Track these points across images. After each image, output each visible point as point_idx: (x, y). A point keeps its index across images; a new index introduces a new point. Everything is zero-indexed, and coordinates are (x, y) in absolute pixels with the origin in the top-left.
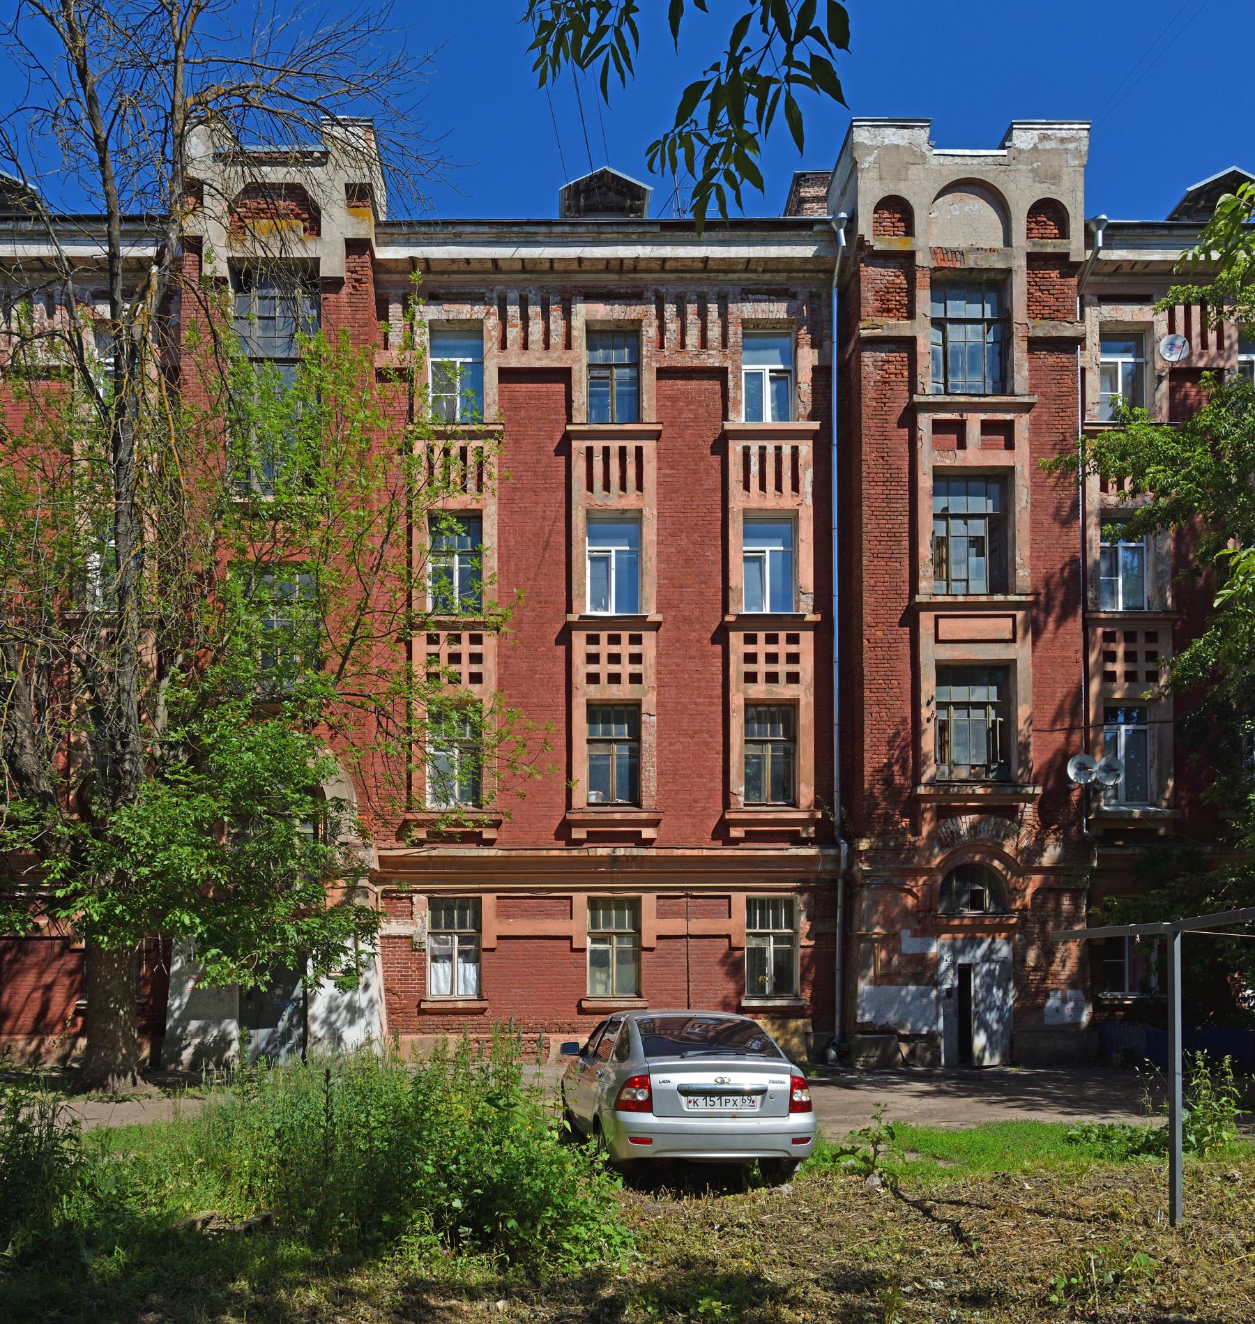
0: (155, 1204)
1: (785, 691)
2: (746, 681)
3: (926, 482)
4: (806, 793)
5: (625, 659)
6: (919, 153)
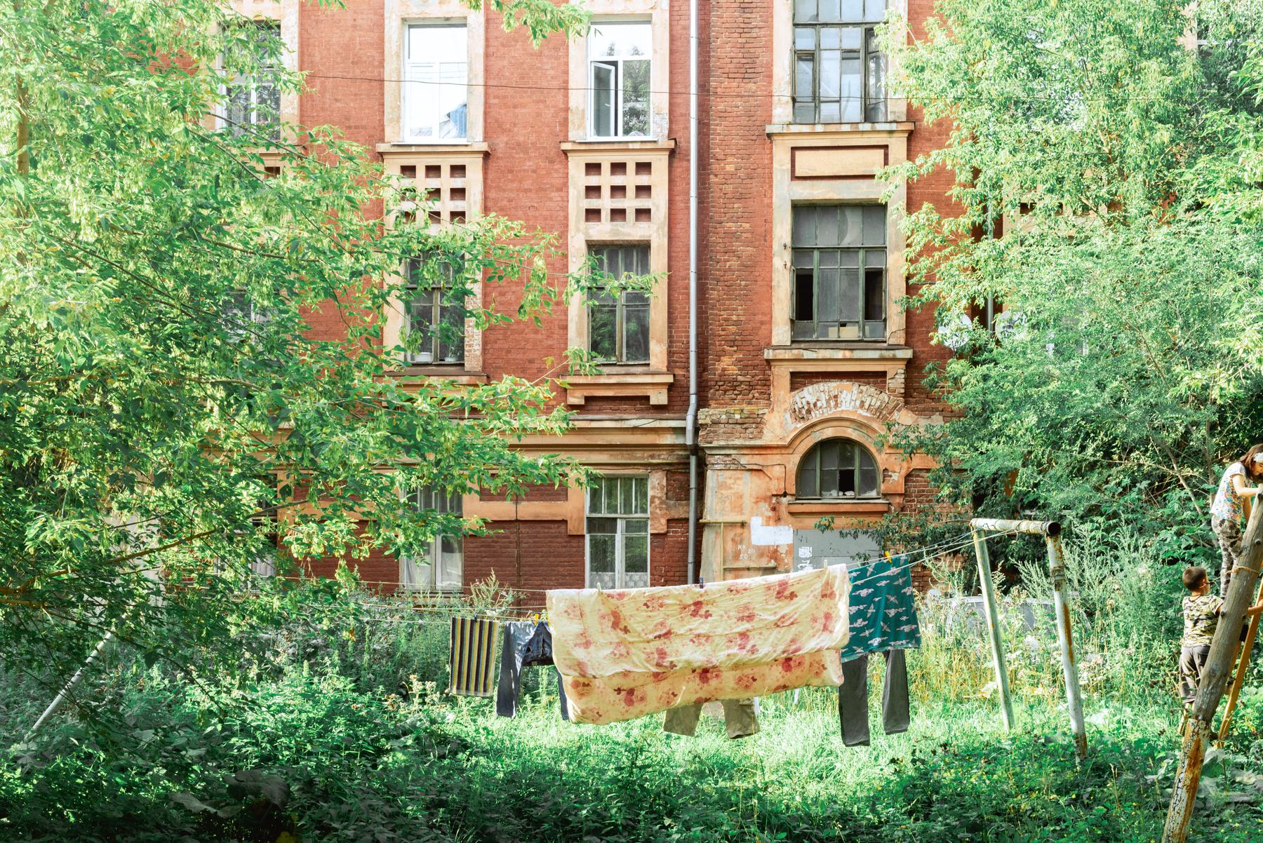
1: (631, 231)
2: (587, 220)
3: (658, 259)
4: (658, 352)
5: (446, 194)
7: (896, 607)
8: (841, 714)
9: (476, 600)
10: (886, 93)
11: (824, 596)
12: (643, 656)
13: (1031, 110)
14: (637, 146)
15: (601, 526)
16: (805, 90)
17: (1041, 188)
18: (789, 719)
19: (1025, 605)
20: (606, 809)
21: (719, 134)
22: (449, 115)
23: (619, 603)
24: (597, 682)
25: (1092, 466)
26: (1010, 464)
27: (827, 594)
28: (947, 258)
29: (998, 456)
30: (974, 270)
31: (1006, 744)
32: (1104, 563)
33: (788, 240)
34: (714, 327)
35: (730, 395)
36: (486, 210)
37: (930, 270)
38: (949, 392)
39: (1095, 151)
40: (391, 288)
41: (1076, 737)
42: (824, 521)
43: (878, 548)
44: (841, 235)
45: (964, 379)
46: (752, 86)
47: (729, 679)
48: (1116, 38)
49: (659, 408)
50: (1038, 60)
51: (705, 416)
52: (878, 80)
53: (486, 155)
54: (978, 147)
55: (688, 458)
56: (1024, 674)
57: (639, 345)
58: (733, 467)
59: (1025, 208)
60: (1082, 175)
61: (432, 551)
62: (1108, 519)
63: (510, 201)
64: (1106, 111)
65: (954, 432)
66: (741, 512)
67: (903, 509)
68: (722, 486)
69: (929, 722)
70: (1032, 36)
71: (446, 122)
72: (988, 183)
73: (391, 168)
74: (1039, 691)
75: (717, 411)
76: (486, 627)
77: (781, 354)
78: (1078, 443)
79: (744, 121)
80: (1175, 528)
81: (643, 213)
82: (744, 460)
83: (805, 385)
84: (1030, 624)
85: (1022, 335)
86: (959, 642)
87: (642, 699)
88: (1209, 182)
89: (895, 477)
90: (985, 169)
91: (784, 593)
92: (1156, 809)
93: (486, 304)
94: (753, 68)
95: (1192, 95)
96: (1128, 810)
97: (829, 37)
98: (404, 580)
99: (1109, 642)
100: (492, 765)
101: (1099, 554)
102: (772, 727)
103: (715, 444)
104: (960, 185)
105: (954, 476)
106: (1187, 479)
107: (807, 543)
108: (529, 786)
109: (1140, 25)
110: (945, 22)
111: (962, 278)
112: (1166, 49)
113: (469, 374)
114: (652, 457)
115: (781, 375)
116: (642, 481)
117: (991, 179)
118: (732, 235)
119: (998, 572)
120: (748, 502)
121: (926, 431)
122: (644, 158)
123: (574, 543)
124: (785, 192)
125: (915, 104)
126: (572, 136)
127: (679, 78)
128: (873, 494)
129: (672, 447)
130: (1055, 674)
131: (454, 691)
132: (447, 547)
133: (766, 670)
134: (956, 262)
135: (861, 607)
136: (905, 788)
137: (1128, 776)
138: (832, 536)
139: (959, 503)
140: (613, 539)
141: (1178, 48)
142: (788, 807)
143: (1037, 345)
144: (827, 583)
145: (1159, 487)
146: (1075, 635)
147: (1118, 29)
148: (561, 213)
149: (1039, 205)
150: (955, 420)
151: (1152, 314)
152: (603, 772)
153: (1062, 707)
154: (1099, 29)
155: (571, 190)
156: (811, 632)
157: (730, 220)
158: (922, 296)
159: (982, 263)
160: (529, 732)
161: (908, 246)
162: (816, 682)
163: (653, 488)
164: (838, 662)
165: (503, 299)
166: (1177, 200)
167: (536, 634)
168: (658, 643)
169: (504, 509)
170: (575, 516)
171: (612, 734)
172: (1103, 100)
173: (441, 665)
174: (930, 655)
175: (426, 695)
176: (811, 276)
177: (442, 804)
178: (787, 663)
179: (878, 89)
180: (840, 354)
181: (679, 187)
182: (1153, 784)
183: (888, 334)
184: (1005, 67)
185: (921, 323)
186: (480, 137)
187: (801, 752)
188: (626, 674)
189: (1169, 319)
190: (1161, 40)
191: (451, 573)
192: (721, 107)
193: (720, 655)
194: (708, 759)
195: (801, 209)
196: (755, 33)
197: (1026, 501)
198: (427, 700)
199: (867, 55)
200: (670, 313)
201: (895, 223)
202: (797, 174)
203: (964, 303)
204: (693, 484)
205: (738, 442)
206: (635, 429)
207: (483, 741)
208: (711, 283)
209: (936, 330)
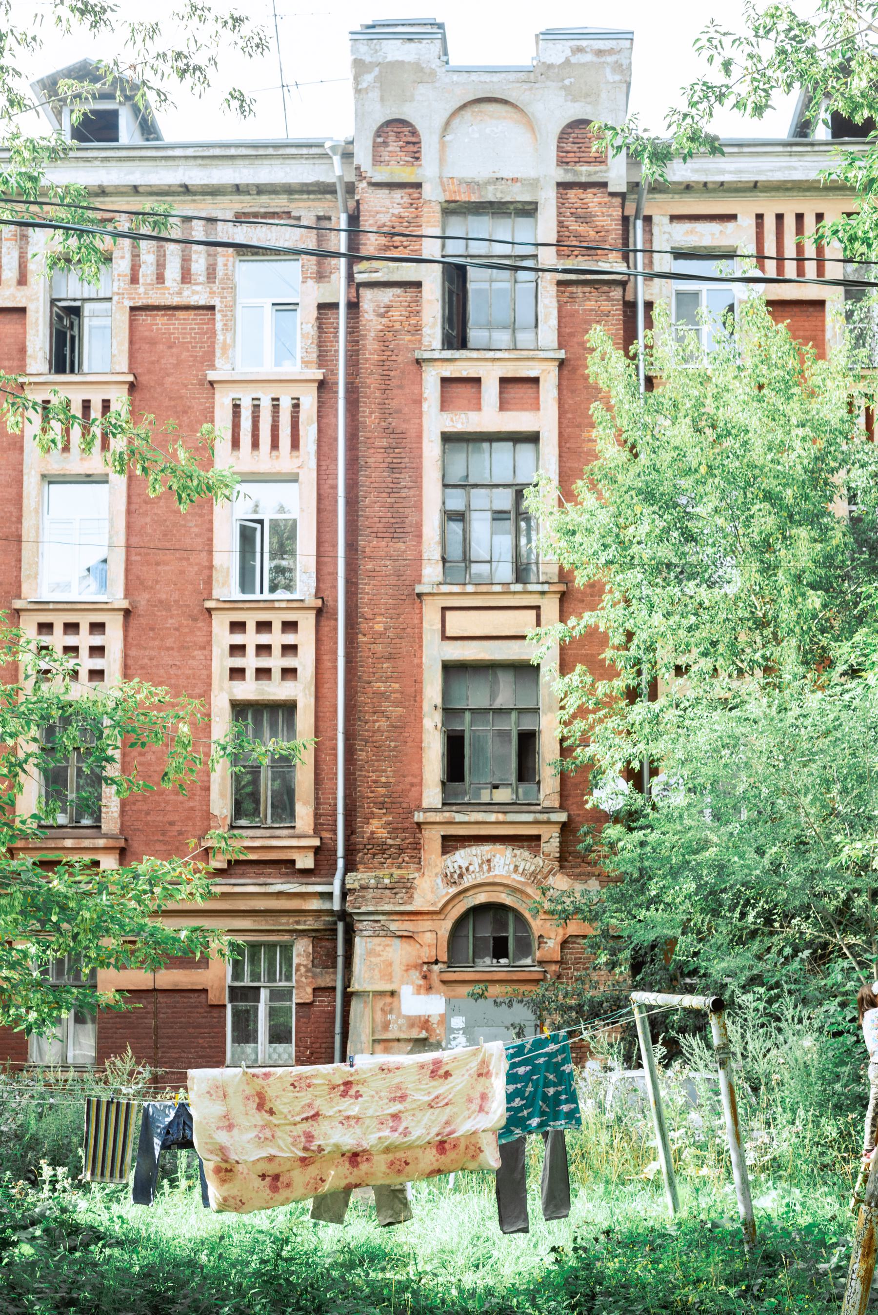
1: (277, 690)
2: (231, 678)
3: (305, 719)
4: (304, 813)
7: (555, 1085)
12: (290, 1140)
14: (283, 605)
15: (244, 995)
16: (455, 552)
17: (695, 651)
18: (444, 1203)
19: (688, 1080)
20: (250, 1306)
23: (264, 1083)
24: (240, 1168)
25: (753, 934)
26: (670, 933)
28: (601, 721)
29: (654, 924)
30: (629, 733)
31: (672, 1230)
32: (768, 1035)
34: (362, 789)
35: (379, 859)
36: (127, 675)
37: (584, 733)
38: (605, 857)
39: (747, 615)
40: (28, 755)
41: (744, 1224)
42: (478, 989)
43: (533, 1017)
44: (493, 696)
45: (620, 844)
46: (401, 546)
47: (380, 1163)
48: (766, 506)
49: (305, 872)
51: (354, 880)
52: (529, 541)
53: (127, 613)
54: (631, 609)
55: (335, 924)
56: (688, 1154)
58: (382, 933)
59: (679, 671)
62: (771, 988)
63: (151, 659)
64: (757, 575)
66: (390, 980)
67: (559, 977)
68: (371, 953)
69: (590, 1205)
70: (683, 500)
71: (84, 577)
73: (28, 629)
74: (705, 1171)
75: (365, 876)
76: (123, 1109)
78: (738, 910)
79: (393, 580)
81: (289, 673)
82: (393, 926)
83: (456, 849)
84: (692, 1102)
85: (679, 799)
86: (620, 1119)
88: (866, 656)
89: (551, 944)
91: (438, 1072)
92: (829, 1301)
93: (124, 770)
94: (403, 527)
95: (843, 561)
96: (801, 1303)
97: (479, 498)
98: (34, 1057)
99: (775, 1119)
101: (762, 1026)
103: (363, 909)
105: (612, 943)
106: (850, 947)
107: (460, 1013)
108: (166, 1280)
109: (789, 492)
110: (595, 486)
111: (617, 741)
113: (106, 836)
114: (298, 923)
115: (432, 839)
116: (287, 949)
117: (645, 642)
118: (382, 695)
119: (658, 1045)
122: (290, 617)
124: (435, 653)
125: (567, 567)
127: (327, 537)
128: (528, 961)
129: (318, 913)
130: (719, 1153)
131: (89, 1177)
132: (79, 1019)
133: (419, 1153)
134: (610, 725)
136: (566, 1280)
137: (800, 1265)
138: (485, 1005)
139: (617, 970)
140: (257, 1008)
141: (829, 514)
142: (443, 1302)
143: (694, 811)
144: (483, 1062)
145: (822, 955)
147: (769, 496)
148: (205, 672)
149: (694, 668)
150: (611, 885)
151: (810, 779)
152: (248, 1263)
153: (729, 1188)
154: (749, 495)
155: (214, 649)
156: (466, 1113)
157: (379, 680)
159: (637, 727)
160: (168, 1220)
161: (562, 708)
162: (472, 1165)
163: (299, 955)
166: (831, 664)
167: (177, 1116)
168: (305, 1126)
173: (73, 1147)
174: (590, 1134)
177: (72, 1302)
178: (441, 1146)
179: (530, 551)
180: (493, 817)
181: (326, 647)
182: (825, 1274)
183: (542, 796)
185: (576, 786)
186: (121, 594)
187: (456, 1240)
188: (271, 1159)
190: (811, 507)
191: (83, 1045)
194: (357, 1247)
195: (450, 669)
196: (404, 493)
197: (686, 971)
198: (58, 1186)
199: (518, 516)
200: (317, 775)
201: (548, 685)
202: (448, 634)
203: (620, 766)
204: (340, 951)
205: (387, 908)
206: (280, 894)
207: (117, 1229)
209: (591, 793)
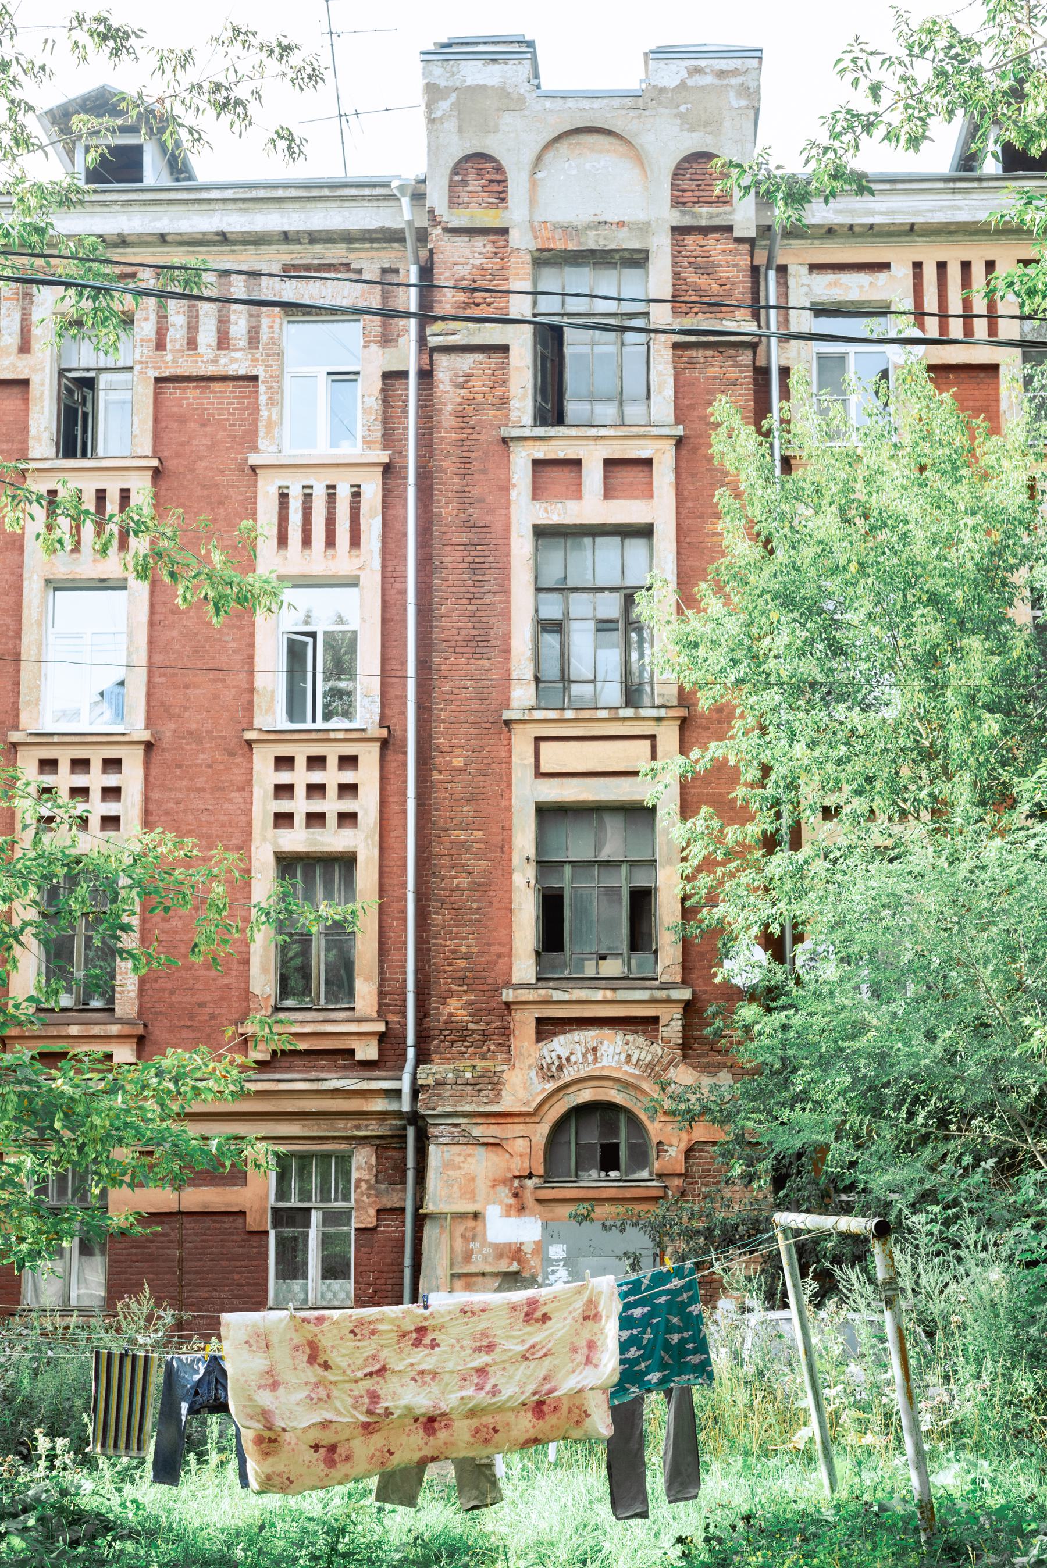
0: (169, 538)
1: (332, 840)
2: (276, 826)
3: (367, 875)
4: (365, 993)
6: (515, 96)
7: (680, 1330)
8: (610, 1475)
9: (124, 1325)
10: (652, 673)
11: (586, 1318)
12: (350, 1401)
13: (834, 693)
14: (341, 735)
15: (289, 1219)
16: (551, 670)
17: (847, 789)
19: (847, 1322)
21: (444, 721)
22: (102, 694)
23: (317, 1329)
24: (287, 1436)
25: (925, 1139)
26: (820, 1138)
27: (590, 1316)
29: (803, 1128)
30: (767, 890)
31: (828, 1514)
33: (531, 851)
34: (438, 961)
35: (459, 1047)
37: (711, 889)
38: (739, 1043)
40: (25, 924)
42: (582, 1209)
43: (651, 1244)
44: (599, 846)
45: (757, 1027)
50: (838, 635)
51: (427, 1074)
52: (642, 656)
53: (149, 746)
54: (768, 738)
55: (404, 1128)
56: (847, 1417)
57: (342, 982)
58: (462, 1140)
59: (827, 813)
60: (897, 773)
61: (67, 1255)
62: (947, 1207)
65: (747, 1095)
66: (473, 1199)
67: (683, 1194)
68: (448, 1165)
69: (725, 1484)
71: (96, 703)
72: (782, 784)
74: (869, 1439)
75: (441, 1068)
76: (141, 1363)
77: (524, 995)
78: (904, 1108)
79: (475, 705)
80: (1033, 1220)
81: (347, 819)
82: (476, 1132)
83: (555, 1034)
85: (830, 971)
86: (761, 1374)
87: (348, 1458)
89: (672, 1152)
90: (777, 765)
91: (534, 1315)
93: (143, 940)
94: (487, 640)
95: (1027, 678)
97: (580, 605)
98: (28, 1298)
99: (955, 1372)
100: (142, 1552)
101: (938, 1254)
102: (517, 1493)
103: (439, 1110)
104: (746, 784)
105: (748, 1151)
107: (560, 1240)
109: (959, 594)
110: (721, 588)
112: (994, 623)
113: (120, 1021)
114: (358, 1128)
115: (524, 1023)
116: (344, 1160)
117: (784, 778)
119: (809, 1280)
120: (482, 1186)
121: (711, 1092)
122: (349, 750)
123: (255, 1241)
124: (527, 793)
125: (688, 687)
126: (258, 723)
127: (393, 652)
128: (645, 1174)
129: (383, 1115)
130: (887, 1416)
132: (85, 1250)
133: (511, 1417)
134: (744, 880)
135: (635, 1332)
139: (755, 1185)
140: (306, 1236)
143: (848, 986)
144: (590, 1301)
146: (912, 1362)
147: (934, 599)
148: (243, 818)
149: (846, 810)
150: (747, 1078)
151: (991, 947)
153: (899, 1461)
154: (910, 598)
155: (256, 790)
158: (701, 921)
159: (776, 882)
160: (194, 1505)
161: (684, 859)
162: (576, 1434)
163: (359, 1168)
164: (605, 1407)
165: (166, 926)
168: (368, 1384)
169: (160, 1197)
170: (256, 1206)
171: (305, 1505)
172: (919, 683)
174: (724, 1393)
175: (55, 1456)
176: (561, 897)
178: (539, 1408)
180: (599, 995)
181: (393, 786)
183: (660, 969)
184: (798, 643)
185: (702, 956)
186: (141, 723)
187: (557, 1528)
188: (325, 1425)
189: (1012, 951)
190: (986, 612)
191: (90, 1282)
192: (446, 688)
193: (451, 1397)
196: (488, 598)
198: (57, 1463)
199: (627, 627)
200: (381, 944)
202: (543, 770)
203: (755, 930)
204: (410, 1163)
205: (468, 1108)
206: (336, 1092)
208: (433, 906)
209: (720, 964)
